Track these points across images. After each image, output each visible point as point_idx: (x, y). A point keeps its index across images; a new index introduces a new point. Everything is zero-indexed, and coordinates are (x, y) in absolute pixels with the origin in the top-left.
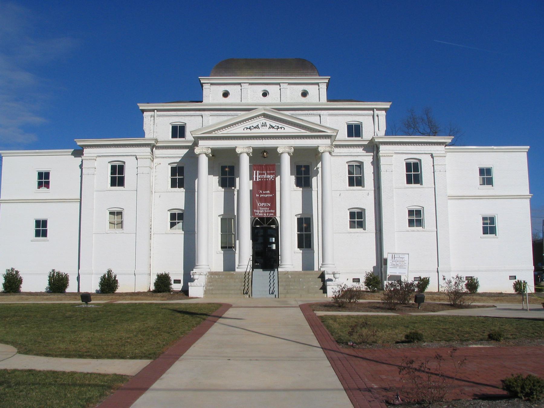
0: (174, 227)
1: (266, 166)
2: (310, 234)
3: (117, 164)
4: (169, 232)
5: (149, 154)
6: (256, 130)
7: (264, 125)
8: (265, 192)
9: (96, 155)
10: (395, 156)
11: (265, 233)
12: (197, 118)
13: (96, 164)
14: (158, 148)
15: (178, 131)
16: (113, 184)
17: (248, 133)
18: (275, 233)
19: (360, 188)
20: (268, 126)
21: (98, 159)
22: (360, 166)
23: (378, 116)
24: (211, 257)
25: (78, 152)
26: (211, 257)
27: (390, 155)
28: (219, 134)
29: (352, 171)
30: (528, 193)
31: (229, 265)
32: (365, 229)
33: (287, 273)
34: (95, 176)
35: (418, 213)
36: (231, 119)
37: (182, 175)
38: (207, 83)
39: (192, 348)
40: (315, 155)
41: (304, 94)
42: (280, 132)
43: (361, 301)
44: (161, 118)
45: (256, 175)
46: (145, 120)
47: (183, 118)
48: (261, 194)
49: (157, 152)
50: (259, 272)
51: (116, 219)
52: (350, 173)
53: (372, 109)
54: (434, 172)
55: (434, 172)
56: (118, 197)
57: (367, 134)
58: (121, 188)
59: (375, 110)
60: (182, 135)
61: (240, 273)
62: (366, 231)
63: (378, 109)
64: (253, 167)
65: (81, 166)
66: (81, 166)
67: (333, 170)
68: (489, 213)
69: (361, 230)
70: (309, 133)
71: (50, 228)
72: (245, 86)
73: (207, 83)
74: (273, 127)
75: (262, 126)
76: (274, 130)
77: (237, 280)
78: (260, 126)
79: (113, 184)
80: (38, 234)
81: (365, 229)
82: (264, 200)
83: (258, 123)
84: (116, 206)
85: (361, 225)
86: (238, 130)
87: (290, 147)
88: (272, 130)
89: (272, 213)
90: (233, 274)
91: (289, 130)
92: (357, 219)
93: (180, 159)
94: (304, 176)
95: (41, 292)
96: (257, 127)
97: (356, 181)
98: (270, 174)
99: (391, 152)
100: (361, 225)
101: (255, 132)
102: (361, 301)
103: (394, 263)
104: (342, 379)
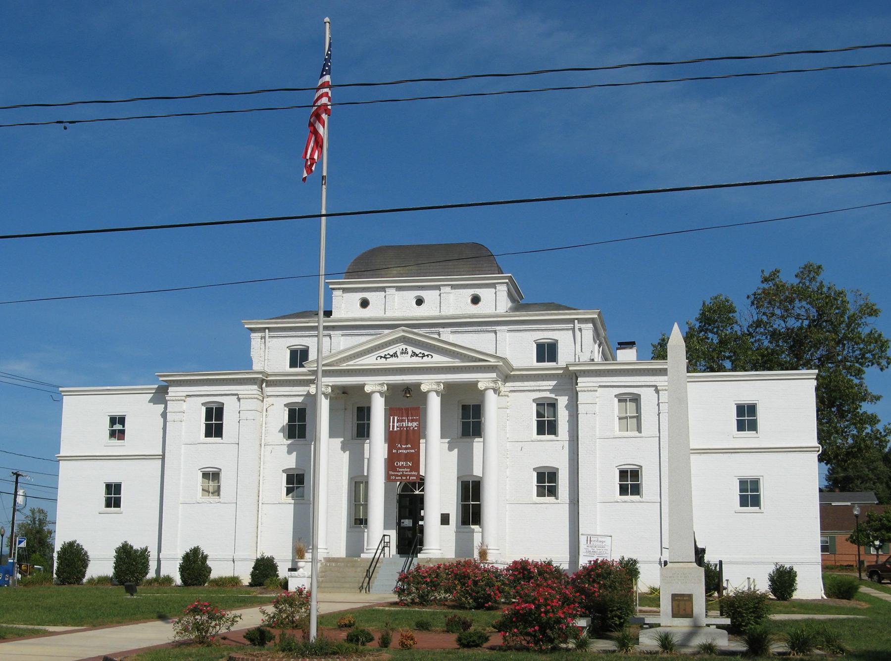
1: (407, 410)
2: (479, 505)
3: (214, 406)
4: (283, 501)
7: (405, 352)
8: (405, 446)
9: (185, 394)
10: (600, 390)
11: (409, 504)
13: (184, 406)
14: (270, 384)
15: (298, 357)
16: (208, 434)
17: (382, 363)
19: (552, 437)
20: (410, 353)
21: (188, 399)
22: (553, 405)
23: (580, 330)
24: (331, 537)
25: (160, 395)
26: (331, 537)
27: (592, 389)
28: (344, 366)
30: (815, 443)
31: (355, 546)
32: (557, 499)
34: (183, 423)
35: (635, 474)
36: (367, 342)
37: (298, 425)
38: (339, 289)
41: (476, 300)
42: (427, 362)
44: (275, 340)
45: (393, 422)
46: (253, 343)
48: (400, 449)
49: (269, 390)
51: (212, 485)
52: (539, 415)
53: (572, 321)
54: (659, 415)
55: (659, 415)
56: (214, 454)
57: (565, 356)
58: (218, 439)
59: (576, 321)
61: (366, 560)
62: (559, 501)
63: (581, 321)
64: (390, 411)
65: (164, 415)
66: (164, 415)
67: (508, 414)
68: (749, 473)
69: (552, 499)
70: (458, 363)
71: (124, 495)
72: (390, 291)
73: (339, 289)
74: (417, 355)
75: (402, 353)
77: (359, 569)
78: (398, 354)
79: (208, 434)
81: (557, 499)
82: (407, 457)
83: (397, 349)
84: (211, 463)
85: (552, 492)
86: (370, 361)
87: (438, 383)
88: (415, 359)
89: (414, 476)
90: (356, 561)
91: (438, 359)
92: (547, 482)
93: (302, 398)
94: (468, 420)
96: (395, 355)
97: (546, 427)
98: (412, 421)
99: (595, 384)
100: (552, 492)
101: (392, 362)
103: (590, 549)
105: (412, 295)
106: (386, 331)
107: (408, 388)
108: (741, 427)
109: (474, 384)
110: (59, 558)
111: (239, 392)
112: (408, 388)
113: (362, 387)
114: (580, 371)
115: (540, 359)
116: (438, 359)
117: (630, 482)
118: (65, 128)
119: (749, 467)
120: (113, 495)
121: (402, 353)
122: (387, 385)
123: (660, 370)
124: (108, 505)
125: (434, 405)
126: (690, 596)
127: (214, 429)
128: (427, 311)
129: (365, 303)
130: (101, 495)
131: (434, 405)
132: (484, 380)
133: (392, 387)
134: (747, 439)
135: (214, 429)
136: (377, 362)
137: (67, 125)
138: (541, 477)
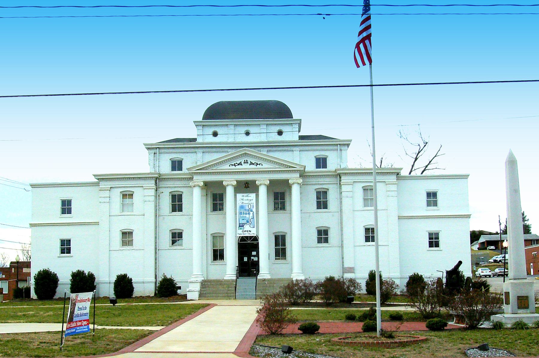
0: (175, 244)
5: (153, 185)
6: (240, 167)
7: (246, 162)
9: (110, 186)
12: (192, 154)
18: (256, 247)
20: (249, 163)
21: (112, 189)
29: (319, 197)
33: (264, 280)
35: (326, 232)
39: (178, 328)
40: (286, 184)
43: (311, 301)
47: (181, 154)
50: (242, 280)
52: (318, 198)
56: (323, 219)
60: (180, 169)
71: (73, 246)
74: (253, 164)
75: (244, 163)
76: (254, 166)
77: (225, 286)
78: (242, 163)
80: (63, 252)
86: (226, 167)
88: (252, 166)
95: (149, 297)
96: (240, 164)
102: (311, 301)
104: (132, 285)
105: (243, 130)
106: (229, 150)
107: (247, 183)
108: (429, 204)
109: (221, 182)
110: (37, 283)
111: (386, 181)
112: (247, 183)
113: (222, 182)
114: (343, 173)
115: (318, 166)
116: (266, 166)
117: (370, 235)
118: (324, 18)
119: (433, 226)
120: (434, 241)
121: (244, 163)
122: (270, 180)
123: (369, 173)
124: (63, 252)
125: (263, 191)
126: (527, 297)
127: (322, 203)
128: (250, 139)
129: (280, 133)
130: (58, 246)
131: (263, 191)
132: (293, 178)
133: (271, 181)
134: (67, 218)
135: (322, 203)
136: (229, 168)
137: (325, 16)
138: (319, 232)
